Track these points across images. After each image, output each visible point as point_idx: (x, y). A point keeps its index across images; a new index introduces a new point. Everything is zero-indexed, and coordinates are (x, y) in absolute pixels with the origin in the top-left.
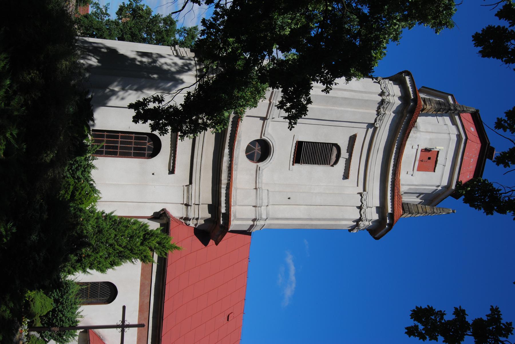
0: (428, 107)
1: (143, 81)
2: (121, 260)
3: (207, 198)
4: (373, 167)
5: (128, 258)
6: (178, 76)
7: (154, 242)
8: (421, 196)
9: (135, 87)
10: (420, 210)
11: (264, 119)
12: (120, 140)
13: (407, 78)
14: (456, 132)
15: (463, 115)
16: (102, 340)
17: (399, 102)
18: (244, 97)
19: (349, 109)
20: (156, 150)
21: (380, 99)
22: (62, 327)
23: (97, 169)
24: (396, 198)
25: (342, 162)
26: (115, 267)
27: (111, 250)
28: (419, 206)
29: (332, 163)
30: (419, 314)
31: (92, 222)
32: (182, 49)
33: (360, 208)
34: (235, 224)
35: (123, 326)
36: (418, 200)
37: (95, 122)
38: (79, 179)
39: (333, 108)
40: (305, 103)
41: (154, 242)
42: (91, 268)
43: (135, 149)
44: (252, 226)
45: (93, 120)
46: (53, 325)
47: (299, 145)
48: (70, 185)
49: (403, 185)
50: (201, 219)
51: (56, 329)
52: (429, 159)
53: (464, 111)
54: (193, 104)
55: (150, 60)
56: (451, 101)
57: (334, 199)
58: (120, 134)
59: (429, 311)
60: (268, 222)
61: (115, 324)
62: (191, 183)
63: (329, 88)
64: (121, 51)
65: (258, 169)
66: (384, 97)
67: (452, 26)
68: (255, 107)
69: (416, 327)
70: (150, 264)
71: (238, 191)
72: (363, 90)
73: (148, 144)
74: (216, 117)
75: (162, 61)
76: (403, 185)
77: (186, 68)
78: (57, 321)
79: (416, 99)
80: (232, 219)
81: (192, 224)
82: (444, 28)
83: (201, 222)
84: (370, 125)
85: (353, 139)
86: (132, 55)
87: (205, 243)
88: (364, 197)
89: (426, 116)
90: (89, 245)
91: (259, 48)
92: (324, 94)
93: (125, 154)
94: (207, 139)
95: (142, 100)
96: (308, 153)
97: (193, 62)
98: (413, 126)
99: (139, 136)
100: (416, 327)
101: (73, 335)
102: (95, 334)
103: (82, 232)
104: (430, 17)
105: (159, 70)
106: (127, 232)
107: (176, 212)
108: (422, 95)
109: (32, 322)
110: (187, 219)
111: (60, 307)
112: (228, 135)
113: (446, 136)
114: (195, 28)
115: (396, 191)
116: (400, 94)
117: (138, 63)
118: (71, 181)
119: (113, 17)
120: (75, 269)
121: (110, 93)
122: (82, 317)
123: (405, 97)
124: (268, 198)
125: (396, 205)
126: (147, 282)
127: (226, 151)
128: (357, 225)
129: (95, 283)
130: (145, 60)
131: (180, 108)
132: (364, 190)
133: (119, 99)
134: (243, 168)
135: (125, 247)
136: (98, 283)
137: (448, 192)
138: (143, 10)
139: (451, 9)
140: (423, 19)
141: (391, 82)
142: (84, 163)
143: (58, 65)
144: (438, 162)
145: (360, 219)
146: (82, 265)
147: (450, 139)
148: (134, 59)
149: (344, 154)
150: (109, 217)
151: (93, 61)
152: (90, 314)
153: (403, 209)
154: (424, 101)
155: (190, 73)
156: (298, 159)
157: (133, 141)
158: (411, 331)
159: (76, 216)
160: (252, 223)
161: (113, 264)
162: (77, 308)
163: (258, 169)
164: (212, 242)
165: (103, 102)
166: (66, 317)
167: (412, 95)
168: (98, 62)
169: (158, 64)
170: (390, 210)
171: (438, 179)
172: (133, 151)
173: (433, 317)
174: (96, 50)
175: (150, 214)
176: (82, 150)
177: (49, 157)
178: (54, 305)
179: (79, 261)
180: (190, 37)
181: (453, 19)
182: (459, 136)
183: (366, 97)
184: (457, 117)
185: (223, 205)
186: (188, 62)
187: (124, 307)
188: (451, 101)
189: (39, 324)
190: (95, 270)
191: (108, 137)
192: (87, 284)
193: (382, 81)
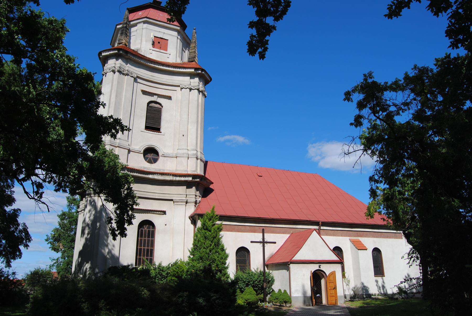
0: (124, 41)
1: (102, 232)
2: (220, 244)
3: (182, 189)
4: (163, 80)
5: (219, 240)
6: (99, 209)
7: (209, 223)
8: (184, 49)
9: (106, 238)
10: (193, 50)
11: (129, 151)
12: (142, 248)
13: (103, 54)
14: (142, 24)
15: (130, 19)
16: (272, 256)
17: (120, 60)
18: (109, 162)
19: (124, 94)
20: (150, 223)
21: (117, 73)
22: (263, 281)
23: (161, 262)
24: (184, 66)
25: (160, 100)
26: (225, 248)
27: (214, 251)
28: (190, 51)
29: (160, 107)
30: (252, 51)
31: (195, 263)
32: (81, 207)
33: (191, 89)
34: (200, 172)
35: (264, 242)
36: (187, 51)
37: (130, 264)
38: (167, 274)
39: (123, 105)
40: (112, 120)
41: (209, 223)
42: (225, 264)
43: (149, 237)
44: (201, 160)
45: (129, 266)
46: (262, 287)
47: (147, 128)
48: (171, 279)
49: (176, 61)
50: (196, 193)
51: (265, 284)
52: (159, 43)
53: (128, 18)
54: (114, 197)
55: (87, 228)
56: (120, 26)
57: (184, 106)
58: (139, 247)
59: (250, 44)
60: (199, 150)
61: (262, 248)
62: (172, 200)
63: (102, 104)
64: (81, 248)
65: (164, 156)
66: (116, 70)
67: (64, 20)
68: (118, 156)
69: (259, 53)
70: (223, 226)
71: (178, 169)
72: (111, 84)
73: (146, 229)
74: (123, 182)
75: (87, 220)
76: (176, 61)
77: (93, 203)
78: (260, 284)
79: (119, 49)
80: (196, 173)
81: (199, 199)
82: (65, 26)
83: (198, 193)
84: (135, 80)
85: (144, 92)
86: (83, 241)
87: (212, 190)
88: (184, 86)
89: (130, 43)
90: (210, 265)
91: (76, 151)
92: (106, 107)
93: (152, 244)
94: (136, 187)
95: (111, 232)
96: (153, 123)
97: (89, 199)
98: (136, 52)
99: (140, 234)
100: (259, 53)
101: (269, 274)
102: (268, 260)
103: (201, 270)
104: (58, 35)
105: (94, 222)
106: (202, 241)
107: (191, 210)
108: (116, 45)
109: (260, 300)
110: (196, 203)
111: (251, 283)
112: (140, 175)
113: (144, 31)
114: (68, 198)
115: (180, 65)
116: (115, 60)
117: (89, 236)
118: (169, 278)
119: (59, 254)
120: (225, 274)
121: (110, 254)
122: (257, 269)
123: (117, 56)
124: (183, 149)
125: (190, 66)
126: (236, 227)
127: (150, 176)
128: (202, 92)
129: (237, 261)
130: (86, 232)
131: (116, 206)
132: (179, 86)
133: (114, 248)
134: (163, 165)
135: (212, 242)
136: (236, 259)
137: (182, 32)
138: (55, 234)
139: (52, 20)
140: (59, 40)
141: (106, 65)
142: (157, 271)
143: (82, 289)
144: (162, 37)
145: (198, 90)
146: (223, 269)
147: (146, 28)
148: (86, 239)
149: (154, 98)
150: (192, 253)
151: (88, 266)
152: (256, 264)
153: (192, 61)
154: (120, 44)
155: (96, 201)
156: (157, 130)
157: (143, 238)
158: (262, 56)
159: (191, 274)
160: (199, 160)
161: (223, 250)
162: (252, 272)
163: (164, 156)
164: (211, 186)
165: (116, 259)
166: (258, 279)
167: (115, 52)
168: (88, 263)
169: (90, 223)
170: (193, 70)
171: (172, 37)
172: (150, 239)
173: (254, 42)
174: (80, 265)
175: (192, 226)
176: (146, 272)
177: (145, 293)
178: (250, 286)
179: (220, 271)
180: (74, 202)
181: (59, 19)
182: (145, 22)
183: (115, 82)
184: (132, 23)
185: (187, 179)
186: (88, 202)
187: (252, 242)
188: (120, 26)
189: (262, 296)
190: (227, 261)
191: (140, 255)
192: (237, 266)
193: (105, 71)
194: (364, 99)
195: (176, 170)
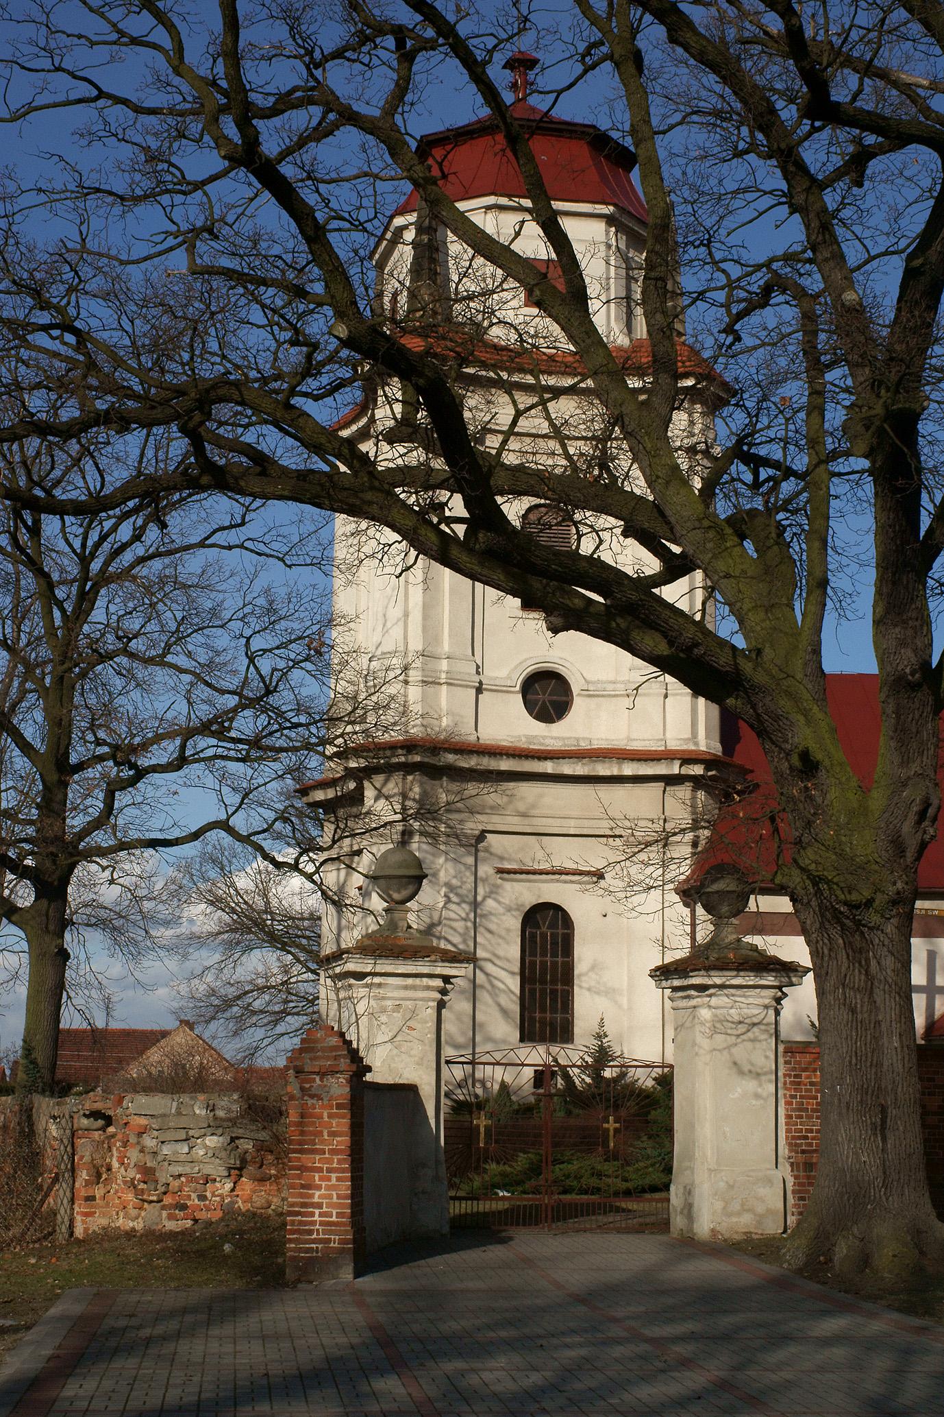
11: (479, 690)
172: (560, 959)
194: (707, 575)
195: (629, 739)
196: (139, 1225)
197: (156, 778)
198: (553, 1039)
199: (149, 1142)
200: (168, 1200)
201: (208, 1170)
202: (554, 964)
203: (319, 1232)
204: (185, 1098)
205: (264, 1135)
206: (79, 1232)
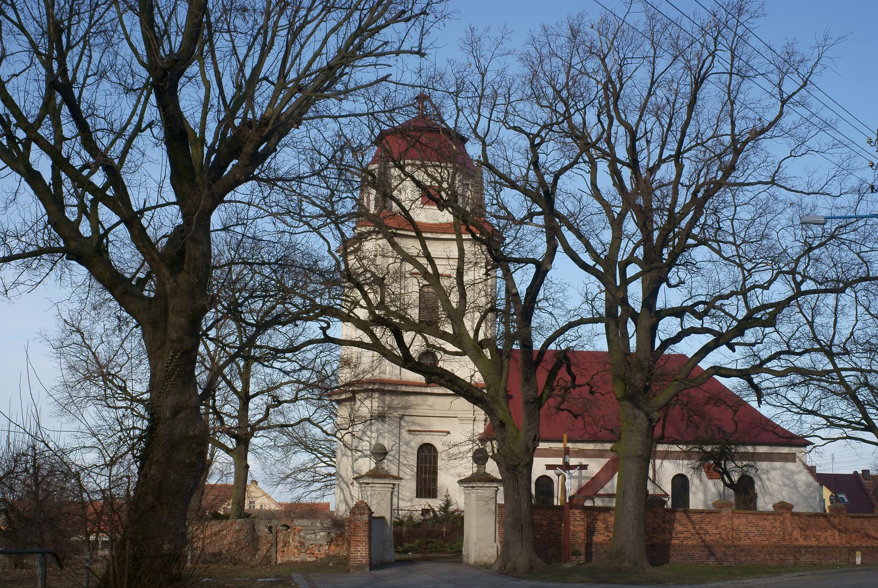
196: (299, 559)
197: (285, 405)
198: (429, 497)
199: (302, 534)
200: (308, 552)
201: (321, 542)
202: (430, 467)
203: (360, 559)
204: (314, 521)
205: (339, 532)
206: (279, 561)
